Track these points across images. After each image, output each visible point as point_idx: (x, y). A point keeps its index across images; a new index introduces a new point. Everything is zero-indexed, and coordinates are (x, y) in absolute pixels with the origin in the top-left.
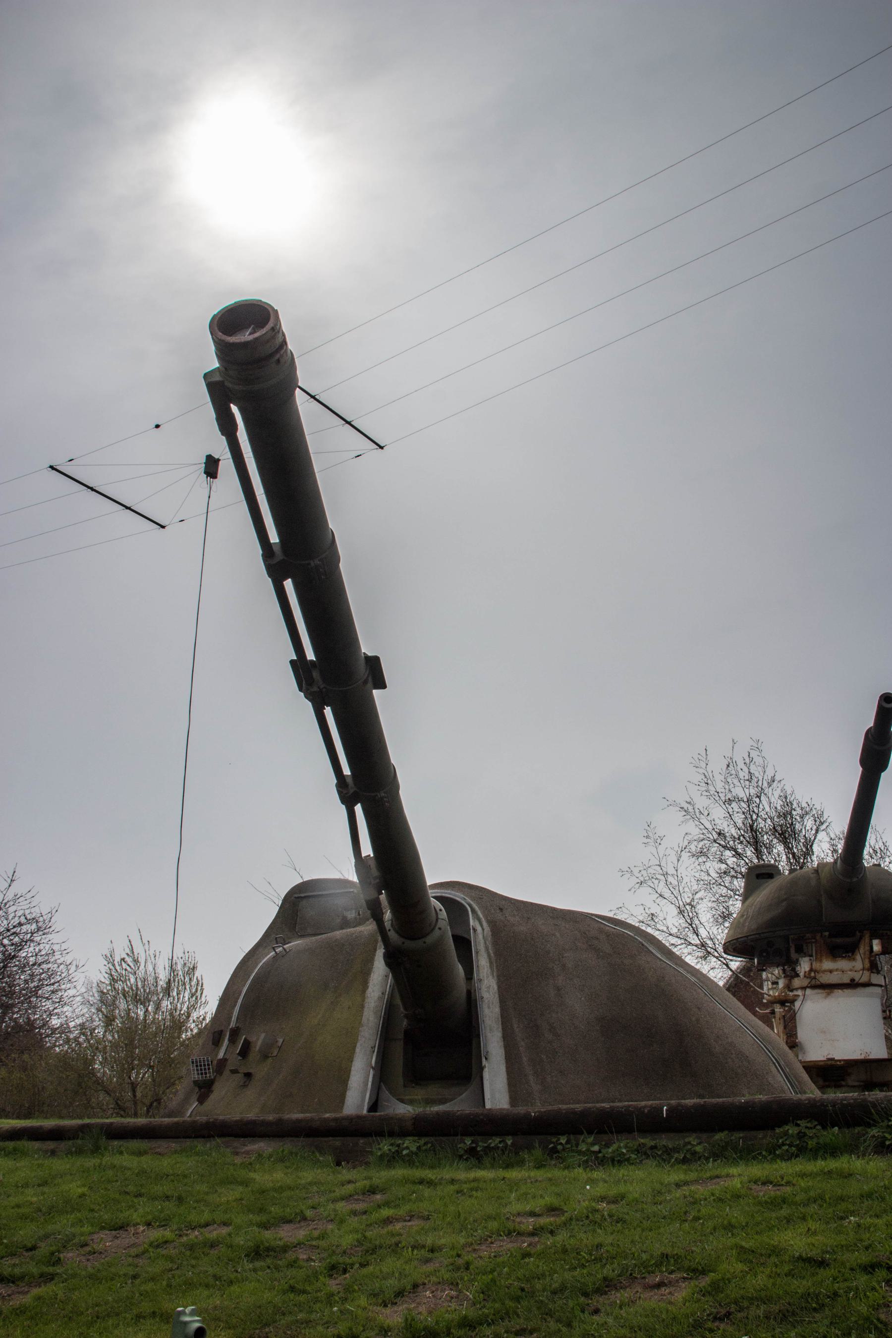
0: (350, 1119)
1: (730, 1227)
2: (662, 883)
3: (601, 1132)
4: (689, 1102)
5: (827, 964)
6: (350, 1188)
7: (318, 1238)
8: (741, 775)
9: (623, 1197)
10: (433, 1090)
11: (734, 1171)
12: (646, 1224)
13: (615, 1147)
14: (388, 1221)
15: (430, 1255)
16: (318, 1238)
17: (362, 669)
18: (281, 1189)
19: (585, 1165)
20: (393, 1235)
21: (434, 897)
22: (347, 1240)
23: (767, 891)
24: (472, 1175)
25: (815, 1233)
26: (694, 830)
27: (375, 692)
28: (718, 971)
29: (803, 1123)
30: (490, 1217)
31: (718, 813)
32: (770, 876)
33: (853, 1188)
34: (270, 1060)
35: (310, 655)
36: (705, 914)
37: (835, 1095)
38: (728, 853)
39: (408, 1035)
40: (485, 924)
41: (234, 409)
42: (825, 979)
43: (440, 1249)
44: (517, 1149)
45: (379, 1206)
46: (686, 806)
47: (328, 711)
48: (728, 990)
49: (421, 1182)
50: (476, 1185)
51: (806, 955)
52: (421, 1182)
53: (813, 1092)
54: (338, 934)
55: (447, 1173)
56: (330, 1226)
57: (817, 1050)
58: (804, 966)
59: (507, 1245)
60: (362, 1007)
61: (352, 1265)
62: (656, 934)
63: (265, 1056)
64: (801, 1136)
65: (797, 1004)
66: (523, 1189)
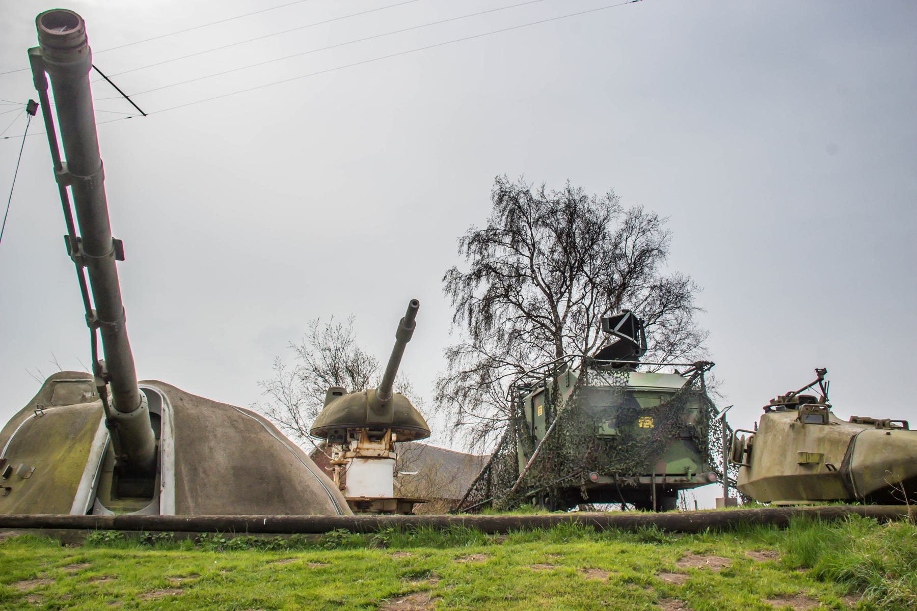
0: (74, 518)
1: (293, 585)
2: (281, 393)
3: (227, 531)
4: (279, 517)
5: (367, 445)
6: (69, 560)
7: (43, 590)
8: (334, 335)
9: (235, 568)
10: (129, 503)
11: (300, 555)
12: (246, 583)
13: (234, 540)
14: (91, 579)
15: (115, 599)
16: (43, 590)
17: (110, 247)
18: (23, 560)
19: (216, 550)
20: (93, 587)
21: (142, 389)
22: (63, 590)
23: (338, 402)
24: (147, 553)
25: (339, 588)
26: (303, 363)
27: (117, 262)
28: (307, 446)
29: (341, 530)
30: (155, 578)
31: (318, 355)
32: (341, 394)
33: (363, 565)
34: (25, 480)
35: (78, 234)
36: (303, 412)
37: (361, 516)
38: (320, 379)
39: (117, 470)
40: (171, 407)
41: (47, 75)
42: (364, 453)
43: (122, 595)
44: (176, 539)
45: (86, 571)
46: (301, 349)
47: (85, 270)
48: (311, 457)
49: (115, 557)
50: (149, 559)
51: (355, 439)
52: (115, 557)
53: (349, 514)
54: (79, 406)
55: (132, 552)
56: (53, 582)
57: (356, 491)
58: (354, 445)
59: (164, 594)
60: (89, 451)
61: (64, 605)
62: (274, 422)
63: (22, 477)
64: (339, 537)
65: (348, 466)
66: (177, 562)
